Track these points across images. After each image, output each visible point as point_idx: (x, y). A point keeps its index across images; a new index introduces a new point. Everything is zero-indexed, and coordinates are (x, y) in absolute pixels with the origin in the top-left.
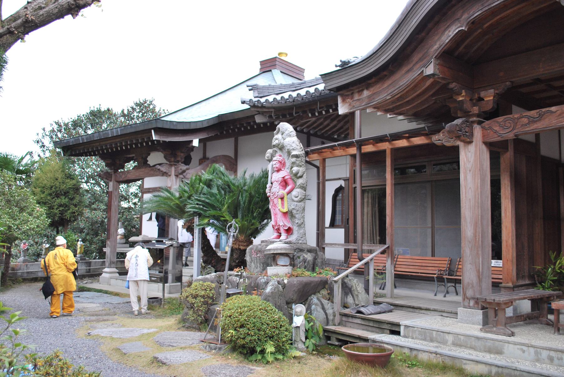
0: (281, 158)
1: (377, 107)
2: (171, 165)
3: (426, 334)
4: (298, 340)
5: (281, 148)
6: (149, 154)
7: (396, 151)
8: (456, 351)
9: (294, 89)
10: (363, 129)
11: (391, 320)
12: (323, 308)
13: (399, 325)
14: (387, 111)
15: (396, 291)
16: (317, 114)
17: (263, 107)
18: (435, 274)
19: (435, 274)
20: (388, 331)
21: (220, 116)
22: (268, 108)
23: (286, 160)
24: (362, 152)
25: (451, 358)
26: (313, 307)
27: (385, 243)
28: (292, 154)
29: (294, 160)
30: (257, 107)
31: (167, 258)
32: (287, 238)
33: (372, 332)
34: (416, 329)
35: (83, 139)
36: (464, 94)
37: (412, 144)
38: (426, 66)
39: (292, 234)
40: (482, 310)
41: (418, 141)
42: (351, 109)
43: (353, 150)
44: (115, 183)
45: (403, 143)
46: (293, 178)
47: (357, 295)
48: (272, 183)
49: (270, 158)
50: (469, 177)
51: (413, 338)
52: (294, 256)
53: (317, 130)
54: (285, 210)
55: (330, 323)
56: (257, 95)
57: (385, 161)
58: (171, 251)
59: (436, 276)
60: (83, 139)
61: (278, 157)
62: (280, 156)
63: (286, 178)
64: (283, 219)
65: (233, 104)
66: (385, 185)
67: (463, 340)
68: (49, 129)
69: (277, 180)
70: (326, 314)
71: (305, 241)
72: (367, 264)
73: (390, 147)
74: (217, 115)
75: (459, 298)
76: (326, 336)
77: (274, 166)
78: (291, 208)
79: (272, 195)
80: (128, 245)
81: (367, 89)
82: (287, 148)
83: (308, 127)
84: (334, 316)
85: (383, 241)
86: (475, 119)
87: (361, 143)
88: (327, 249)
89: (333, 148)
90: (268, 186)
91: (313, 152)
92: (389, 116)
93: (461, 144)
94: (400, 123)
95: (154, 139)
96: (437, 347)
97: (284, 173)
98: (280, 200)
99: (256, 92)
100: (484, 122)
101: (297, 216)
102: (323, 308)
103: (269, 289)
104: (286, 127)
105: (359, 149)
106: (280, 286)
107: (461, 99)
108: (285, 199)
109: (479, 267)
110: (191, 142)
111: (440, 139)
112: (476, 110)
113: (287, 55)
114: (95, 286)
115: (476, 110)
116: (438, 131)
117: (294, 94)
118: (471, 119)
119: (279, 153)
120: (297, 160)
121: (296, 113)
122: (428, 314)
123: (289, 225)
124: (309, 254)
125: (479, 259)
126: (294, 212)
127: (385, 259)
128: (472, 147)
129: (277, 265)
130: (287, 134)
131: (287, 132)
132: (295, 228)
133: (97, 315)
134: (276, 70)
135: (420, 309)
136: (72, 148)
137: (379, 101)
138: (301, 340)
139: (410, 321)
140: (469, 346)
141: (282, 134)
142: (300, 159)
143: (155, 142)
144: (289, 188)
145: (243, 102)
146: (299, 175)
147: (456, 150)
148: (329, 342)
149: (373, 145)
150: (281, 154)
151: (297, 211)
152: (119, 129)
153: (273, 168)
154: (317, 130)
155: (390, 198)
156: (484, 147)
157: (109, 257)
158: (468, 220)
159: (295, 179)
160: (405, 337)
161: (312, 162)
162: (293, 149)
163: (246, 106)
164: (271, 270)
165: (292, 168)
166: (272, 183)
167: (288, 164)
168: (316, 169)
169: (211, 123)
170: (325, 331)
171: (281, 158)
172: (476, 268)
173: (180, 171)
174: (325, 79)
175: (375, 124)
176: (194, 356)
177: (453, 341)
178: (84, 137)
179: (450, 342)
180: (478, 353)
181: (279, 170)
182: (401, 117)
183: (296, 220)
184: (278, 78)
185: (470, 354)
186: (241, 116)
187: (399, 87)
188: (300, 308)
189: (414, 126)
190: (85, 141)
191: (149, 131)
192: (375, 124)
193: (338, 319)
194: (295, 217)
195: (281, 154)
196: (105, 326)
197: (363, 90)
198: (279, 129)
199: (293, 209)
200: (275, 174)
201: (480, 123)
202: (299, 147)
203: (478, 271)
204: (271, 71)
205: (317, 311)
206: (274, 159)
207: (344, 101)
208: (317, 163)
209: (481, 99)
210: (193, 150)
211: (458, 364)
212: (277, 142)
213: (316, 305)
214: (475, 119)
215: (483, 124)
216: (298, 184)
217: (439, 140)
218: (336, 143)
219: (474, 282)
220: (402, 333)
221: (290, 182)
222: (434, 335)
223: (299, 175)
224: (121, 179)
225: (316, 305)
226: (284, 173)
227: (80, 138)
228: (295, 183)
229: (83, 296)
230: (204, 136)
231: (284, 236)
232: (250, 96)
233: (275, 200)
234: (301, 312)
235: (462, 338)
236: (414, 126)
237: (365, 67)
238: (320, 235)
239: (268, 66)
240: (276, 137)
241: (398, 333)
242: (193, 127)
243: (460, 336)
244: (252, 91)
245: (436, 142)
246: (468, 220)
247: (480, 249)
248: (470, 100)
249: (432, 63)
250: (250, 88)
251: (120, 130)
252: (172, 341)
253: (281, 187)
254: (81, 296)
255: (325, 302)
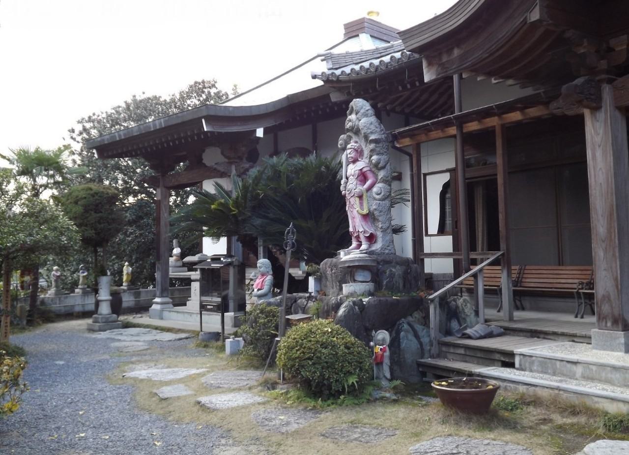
0: (357, 145)
1: (475, 69)
2: (231, 163)
3: (547, 365)
4: (381, 376)
5: (356, 131)
6: (204, 151)
7: (510, 130)
8: (585, 385)
9: (379, 55)
10: (466, 102)
11: (503, 348)
12: (417, 336)
13: (512, 355)
14: (490, 74)
15: (517, 314)
16: (409, 86)
17: (338, 81)
18: (575, 289)
19: (575, 289)
20: (500, 364)
21: (289, 98)
22: (345, 82)
23: (363, 147)
24: (464, 131)
25: (461, 356)
26: (402, 334)
27: (499, 250)
28: (371, 138)
29: (372, 146)
30: (332, 81)
31: (226, 282)
32: (370, 247)
33: (478, 364)
34: (534, 358)
35: (120, 136)
36: (585, 44)
37: (528, 117)
38: (530, 9)
39: (375, 242)
40: (622, 331)
41: (534, 112)
42: (438, 75)
43: (453, 131)
44: (164, 189)
45: (515, 116)
46: (373, 169)
47: (464, 319)
48: (347, 178)
49: (343, 146)
50: (599, 153)
51: (531, 371)
52: (378, 270)
53: (413, 107)
54: (365, 212)
55: (427, 355)
56: (331, 66)
57: (494, 144)
58: (231, 271)
59: (576, 291)
60: (120, 136)
61: (353, 144)
62: (356, 142)
63: (365, 170)
64: (363, 223)
65: (303, 82)
66: (496, 175)
67: (596, 371)
68: (78, 128)
69: (353, 173)
70: (421, 344)
71: (393, 251)
72: (475, 276)
73: (500, 122)
74: (285, 96)
75: (594, 319)
76: (421, 372)
77: (349, 156)
78: (372, 209)
79: (347, 193)
80: (186, 269)
81: (458, 46)
82: (363, 132)
83: (401, 104)
84: (432, 345)
85: (493, 245)
86: (603, 76)
87: (462, 120)
88: (427, 261)
89: (427, 129)
90: (342, 182)
91: (402, 135)
92: (494, 81)
93: (587, 113)
94: (508, 91)
95: (205, 130)
96: (561, 381)
97: (361, 164)
98: (357, 199)
99: (330, 63)
100: (615, 80)
101: (380, 219)
102: (417, 336)
103: (341, 311)
104: (358, 103)
105: (460, 128)
106: (357, 307)
107: (582, 51)
108: (364, 197)
109: (617, 272)
110: (255, 131)
111: (559, 107)
112: (603, 64)
113: (378, 14)
114: (143, 319)
115: (603, 64)
116: (555, 97)
117: (376, 62)
118: (597, 78)
119: (355, 138)
120: (376, 147)
121: (380, 86)
122: (555, 340)
123: (371, 230)
124: (398, 267)
125: (616, 263)
126: (376, 213)
127: (500, 272)
128: (601, 115)
129: (355, 281)
130: (361, 114)
131: (362, 111)
132: (379, 234)
133: (138, 355)
134: (364, 34)
135: (555, 334)
136: (108, 147)
137: (474, 61)
138: (385, 376)
139: (526, 349)
140: (603, 378)
141: (356, 114)
142: (381, 145)
143: (209, 134)
144: (368, 183)
145: (314, 77)
146: (380, 165)
147: (580, 121)
148: (424, 379)
149: (479, 121)
150: (358, 140)
151: (381, 212)
152: (162, 120)
153: (347, 158)
154: (413, 107)
155: (503, 189)
156: (618, 114)
157: (160, 283)
158: (600, 212)
159: (376, 171)
160: (521, 369)
161: (405, 149)
162: (372, 133)
163: (319, 83)
164: (347, 289)
165: (371, 156)
166: (347, 178)
167: (366, 153)
168: (408, 157)
169: (279, 107)
170: (420, 365)
171: (357, 145)
172: (613, 275)
173: (242, 171)
174: (403, 38)
175: (487, 96)
176: (247, 399)
177: (582, 374)
178: (122, 133)
179: (578, 375)
180: (616, 388)
181: (355, 161)
182: (510, 82)
183: (380, 223)
184: (365, 43)
185: (603, 389)
186: (316, 95)
187: (497, 41)
188: (383, 335)
189: (529, 91)
190: (123, 137)
191: (200, 119)
192: (487, 96)
193: (435, 350)
194: (378, 220)
195: (358, 140)
196: (146, 368)
197: (452, 49)
198: (352, 107)
199: (375, 209)
200: (351, 166)
201: (610, 81)
202: (378, 130)
203: (616, 279)
204: (358, 36)
205: (407, 339)
206: (349, 146)
207: (430, 64)
208: (410, 151)
209: (611, 50)
210: (258, 143)
211: (588, 402)
212: (350, 124)
213: (406, 331)
214: (603, 76)
215: (615, 83)
216: (380, 177)
217: (559, 108)
218: (429, 122)
219: (611, 294)
220: (517, 365)
221: (369, 175)
222: (558, 366)
223: (380, 165)
224: (171, 185)
225: (406, 331)
226: (361, 164)
227: (116, 134)
228: (376, 176)
229: (126, 333)
230: (270, 123)
231: (364, 246)
232: (322, 67)
233: (352, 200)
234: (384, 340)
235: (594, 368)
236: (529, 91)
237: (453, 18)
238: (418, 243)
239: (353, 30)
240: (349, 117)
241: (511, 365)
242: (255, 113)
243: (591, 366)
244: (325, 62)
245: (555, 111)
246: (600, 212)
247: (617, 250)
248: (596, 52)
249: (538, 7)
250: (323, 58)
251: (164, 122)
252: (223, 382)
253: (359, 183)
254: (124, 333)
255: (418, 327)
